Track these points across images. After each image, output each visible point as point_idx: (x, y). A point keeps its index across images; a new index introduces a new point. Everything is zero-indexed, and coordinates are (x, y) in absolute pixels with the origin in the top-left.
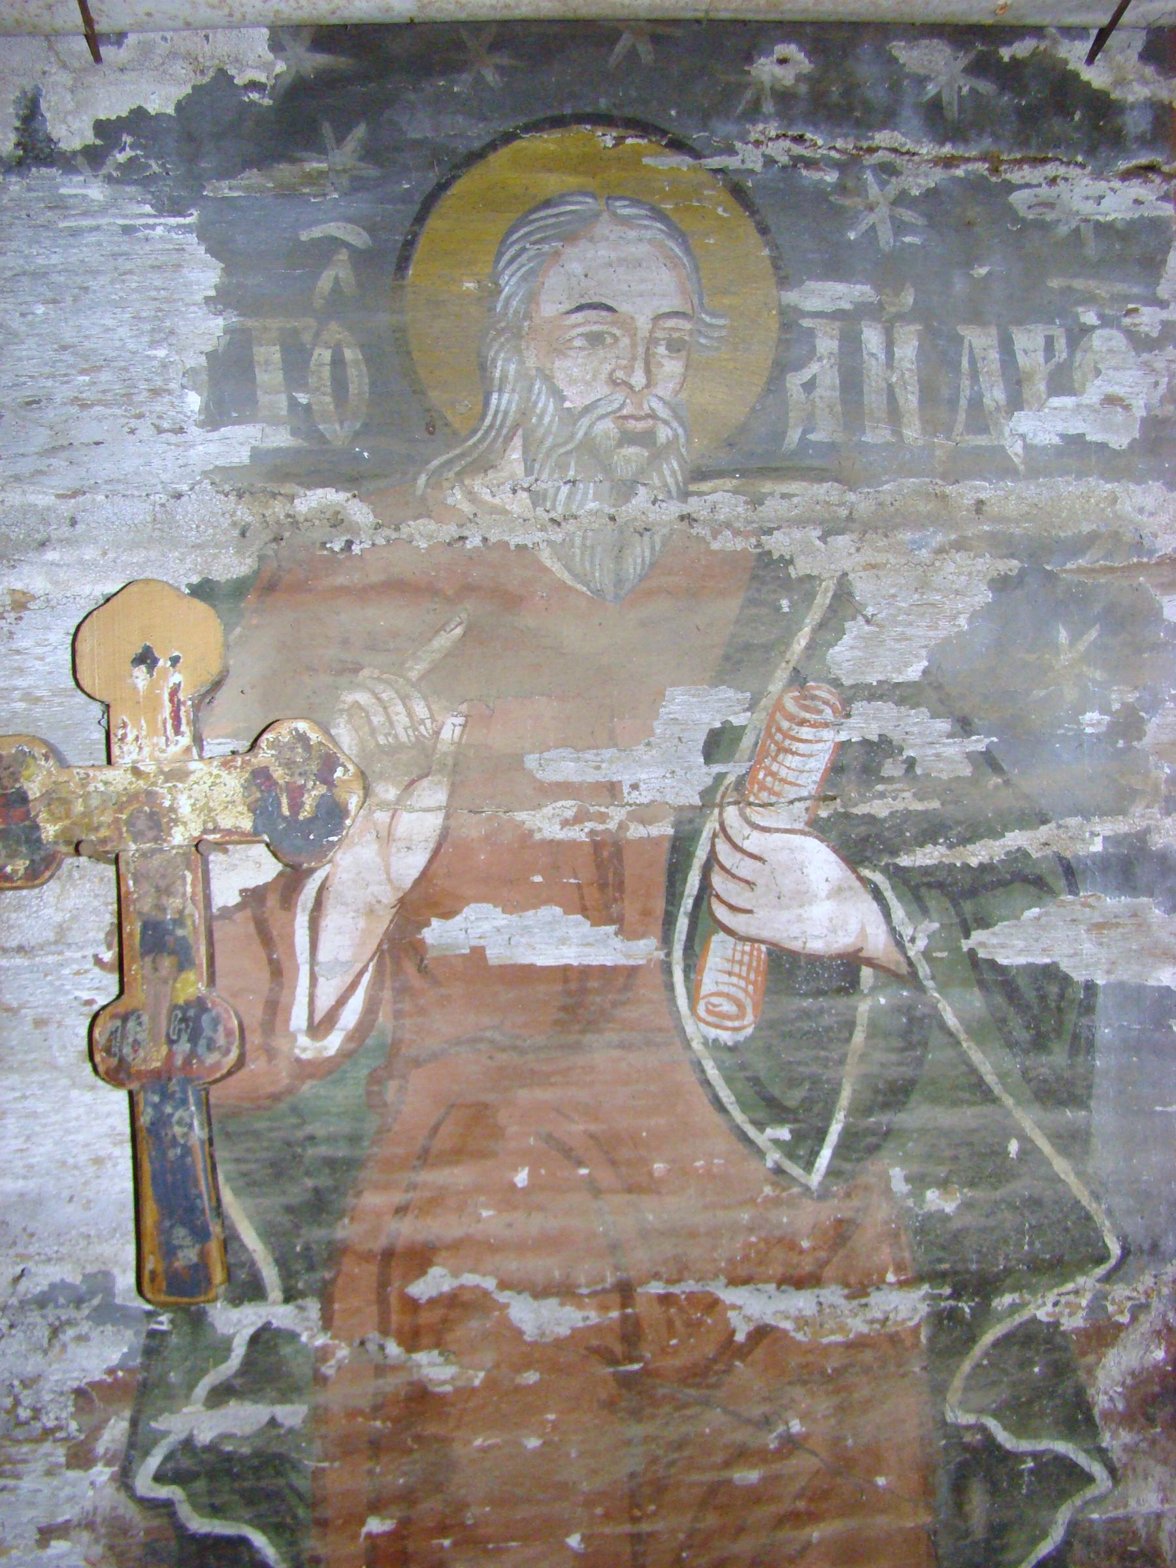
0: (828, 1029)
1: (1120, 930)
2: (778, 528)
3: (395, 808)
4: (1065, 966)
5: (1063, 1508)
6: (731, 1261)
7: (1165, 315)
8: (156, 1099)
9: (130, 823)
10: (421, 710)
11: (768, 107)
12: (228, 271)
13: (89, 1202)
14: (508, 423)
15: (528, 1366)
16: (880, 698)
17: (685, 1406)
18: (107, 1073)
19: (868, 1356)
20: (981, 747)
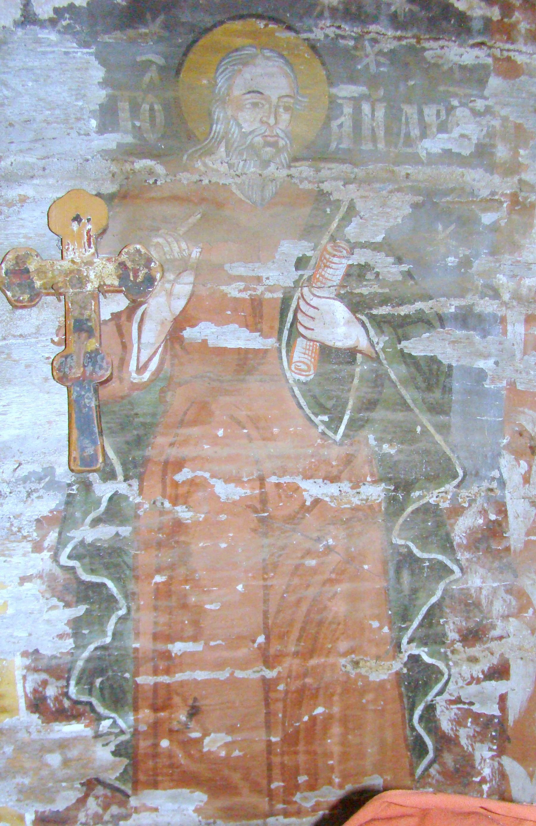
0: (344, 377)
1: (462, 344)
2: (326, 181)
3: (173, 283)
4: (440, 357)
5: (442, 583)
6: (304, 469)
7: (487, 103)
8: (78, 389)
9: (70, 281)
10: (184, 245)
11: (327, 14)
12: (108, 72)
13: (46, 439)
14: (220, 137)
15: (222, 512)
16: (366, 248)
17: (286, 532)
18: (59, 379)
19: (360, 514)
20: (406, 269)
